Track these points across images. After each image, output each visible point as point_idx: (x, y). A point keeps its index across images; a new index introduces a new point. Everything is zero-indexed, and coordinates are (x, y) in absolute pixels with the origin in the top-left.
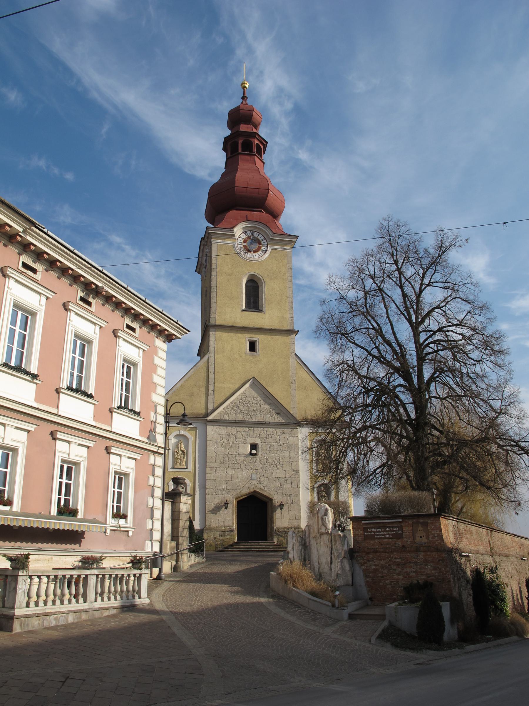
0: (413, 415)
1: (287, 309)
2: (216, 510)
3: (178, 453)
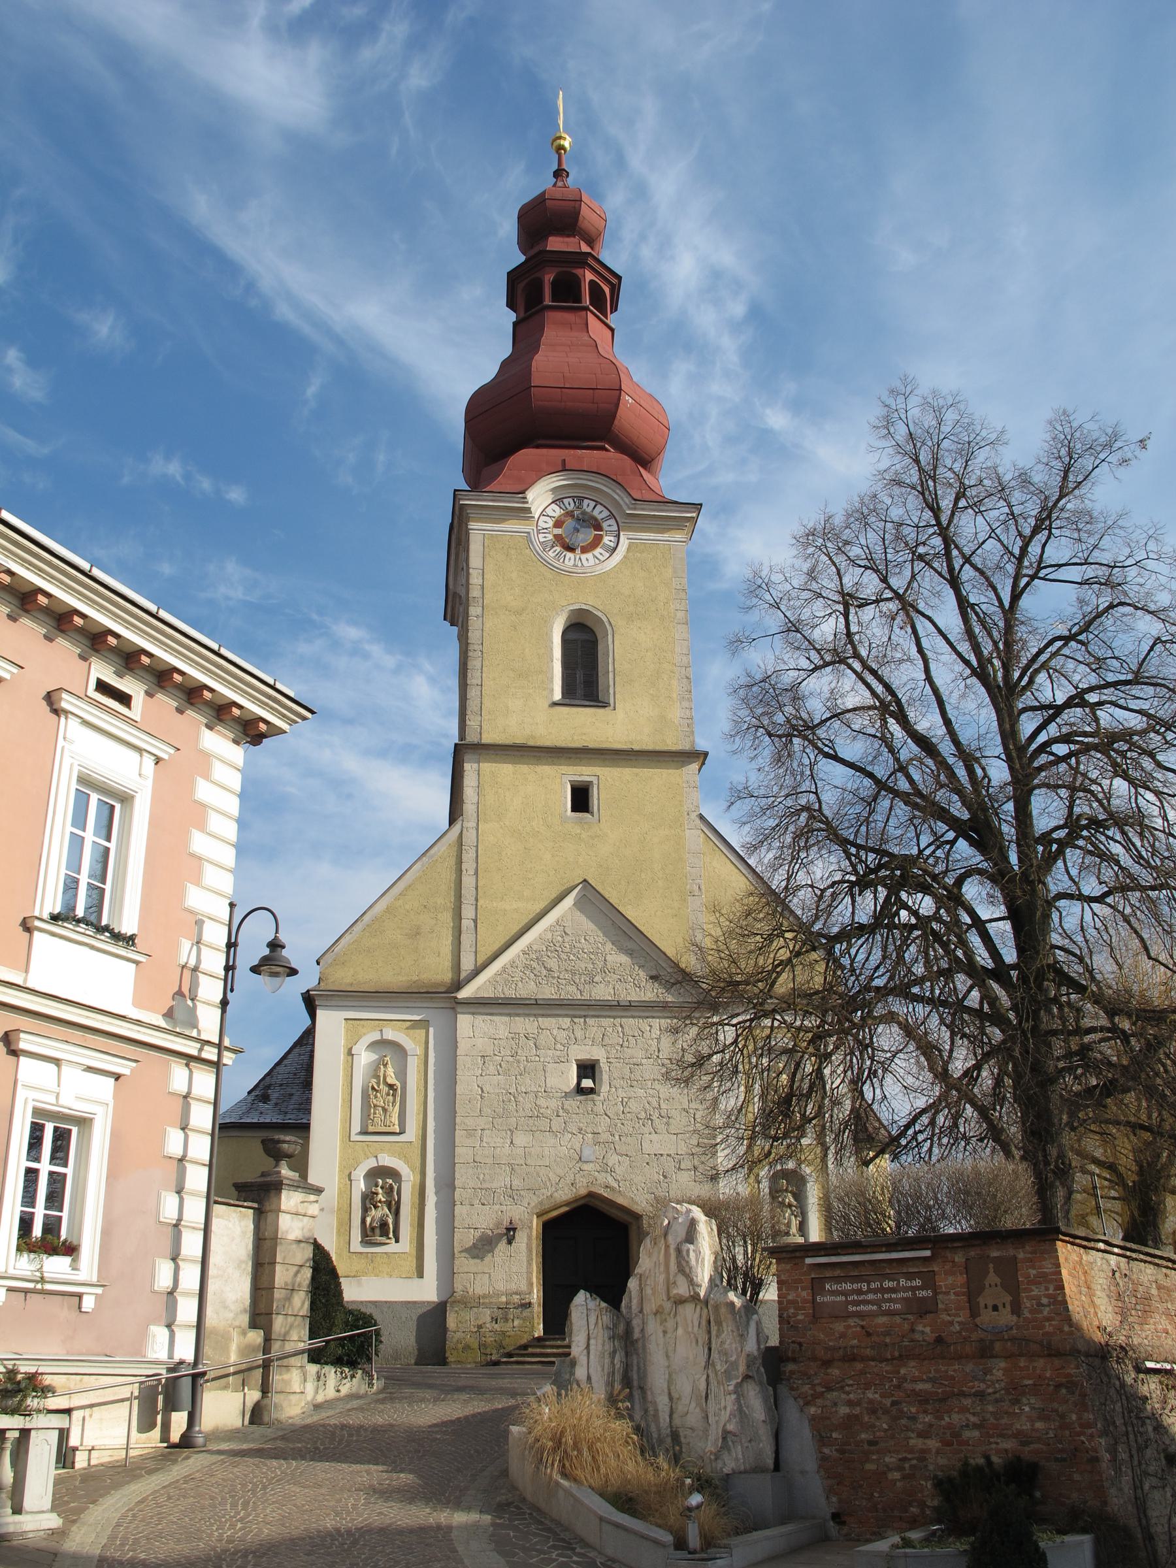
0: (1010, 956)
1: (675, 696)
2: (483, 1246)
3: (377, 1091)
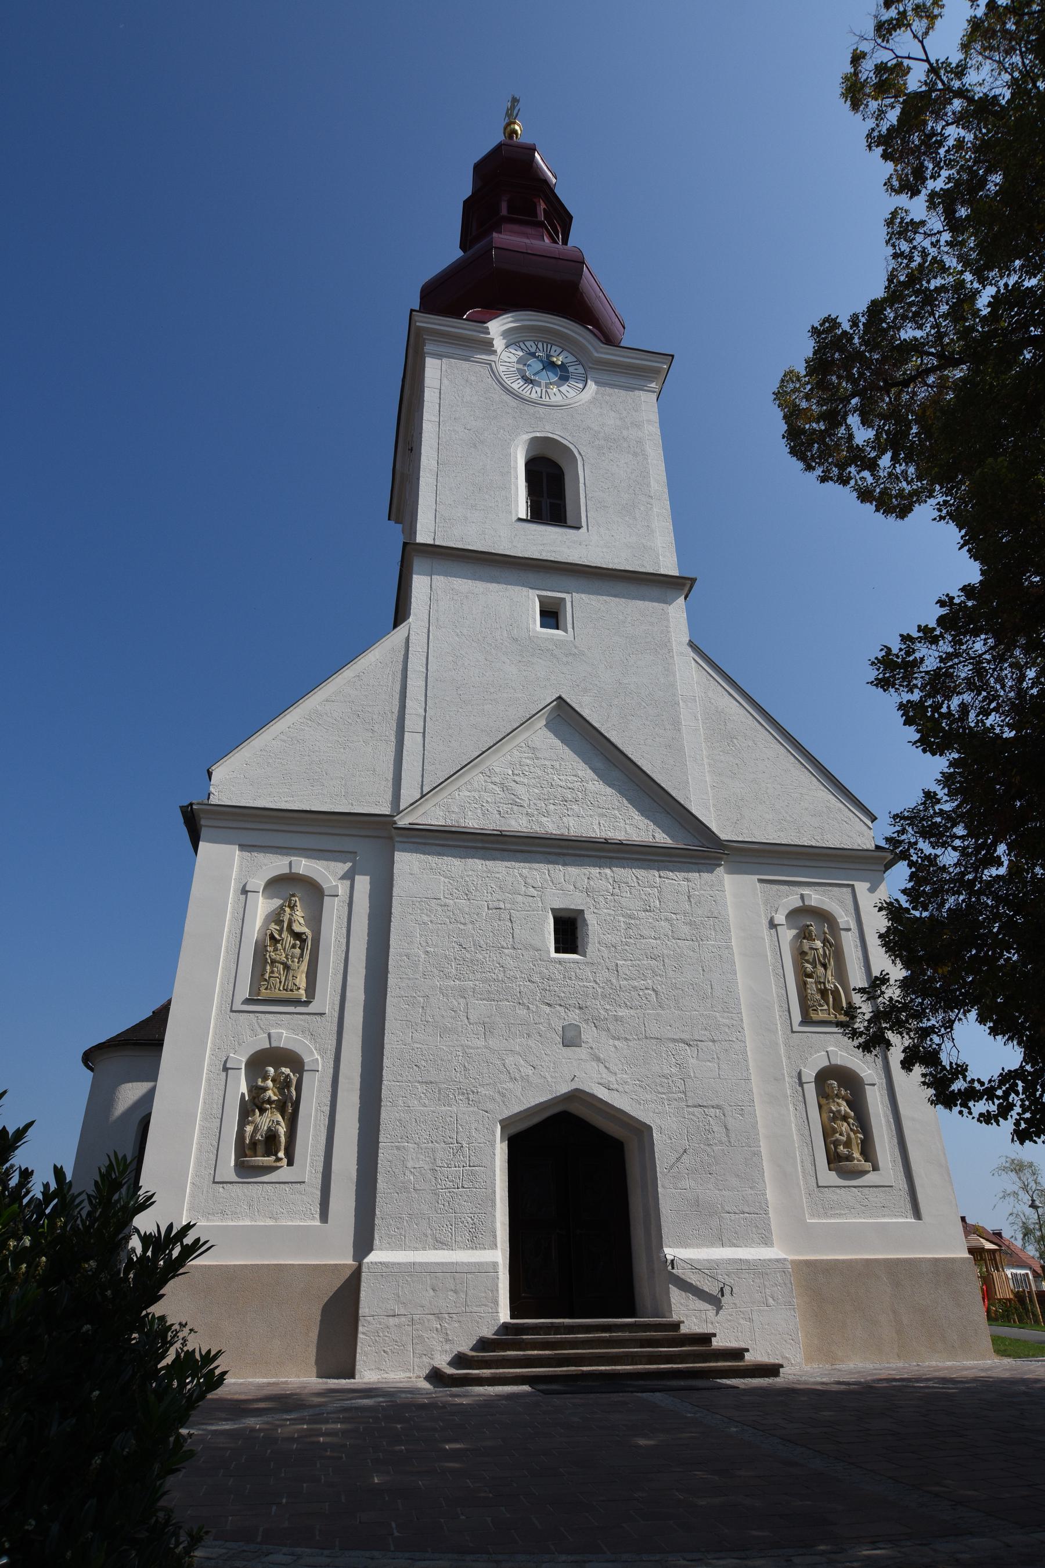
3: (277, 941)
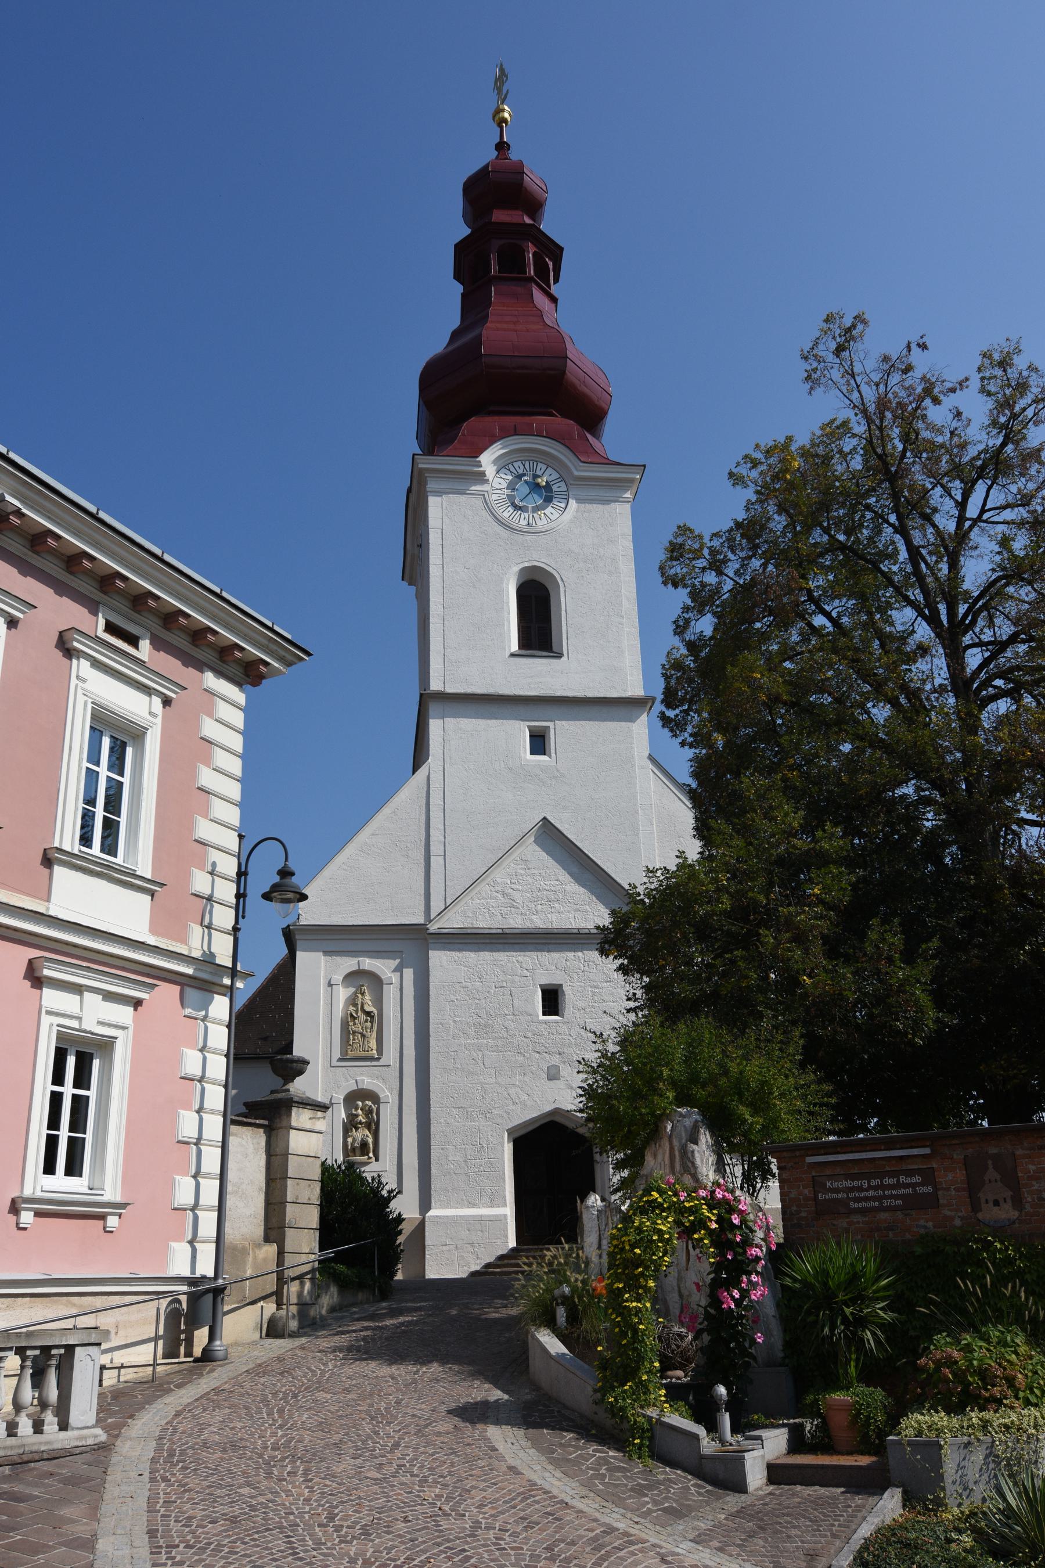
3: (355, 1018)
